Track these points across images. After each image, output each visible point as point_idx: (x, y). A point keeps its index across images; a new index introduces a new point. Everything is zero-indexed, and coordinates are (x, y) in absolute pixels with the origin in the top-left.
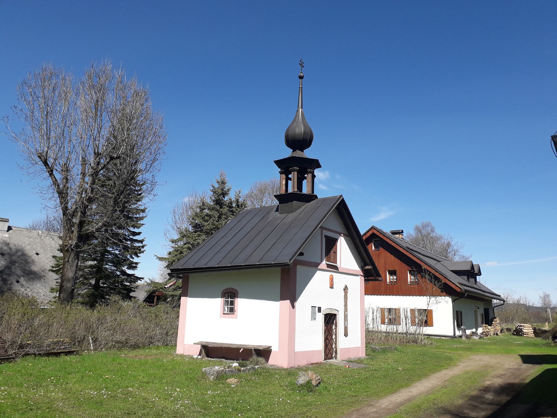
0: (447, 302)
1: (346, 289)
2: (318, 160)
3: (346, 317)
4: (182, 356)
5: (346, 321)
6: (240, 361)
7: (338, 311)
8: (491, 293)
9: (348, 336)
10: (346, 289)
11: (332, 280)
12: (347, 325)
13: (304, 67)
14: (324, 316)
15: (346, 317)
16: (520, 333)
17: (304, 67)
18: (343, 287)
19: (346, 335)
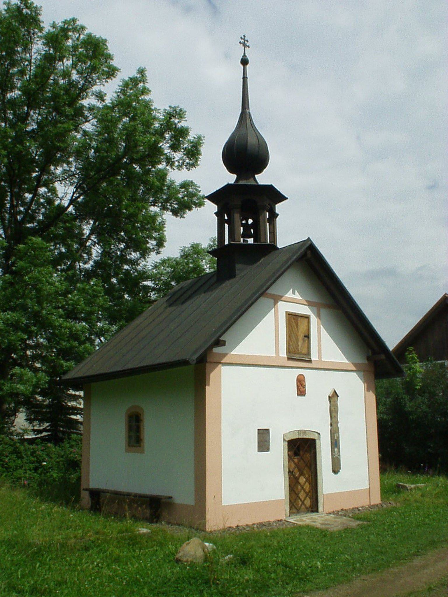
0: (215, 210)
1: (334, 397)
2: (271, 186)
3: (335, 444)
4: (393, 350)
5: (336, 449)
6: (83, 557)
7: (319, 434)
8: (196, 291)
9: (339, 471)
10: (334, 397)
11: (301, 383)
12: (339, 455)
13: (249, 47)
14: (287, 443)
15: (335, 444)
16: (98, 225)
17: (249, 47)
18: (329, 393)
19: (335, 471)
